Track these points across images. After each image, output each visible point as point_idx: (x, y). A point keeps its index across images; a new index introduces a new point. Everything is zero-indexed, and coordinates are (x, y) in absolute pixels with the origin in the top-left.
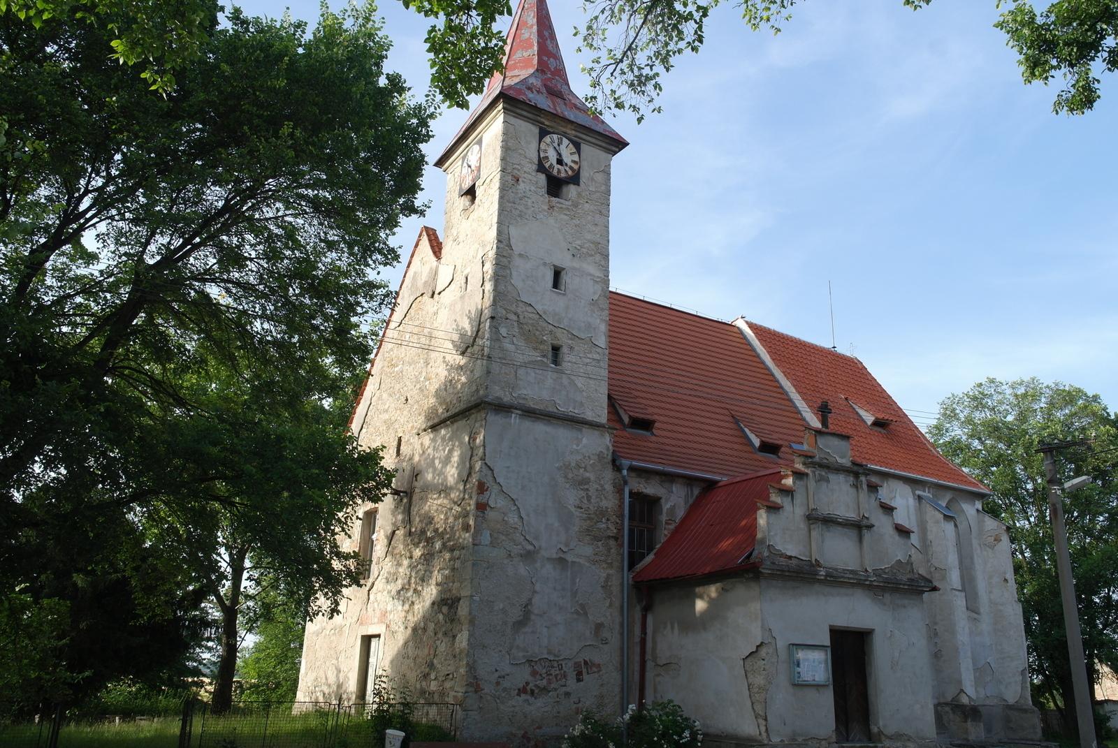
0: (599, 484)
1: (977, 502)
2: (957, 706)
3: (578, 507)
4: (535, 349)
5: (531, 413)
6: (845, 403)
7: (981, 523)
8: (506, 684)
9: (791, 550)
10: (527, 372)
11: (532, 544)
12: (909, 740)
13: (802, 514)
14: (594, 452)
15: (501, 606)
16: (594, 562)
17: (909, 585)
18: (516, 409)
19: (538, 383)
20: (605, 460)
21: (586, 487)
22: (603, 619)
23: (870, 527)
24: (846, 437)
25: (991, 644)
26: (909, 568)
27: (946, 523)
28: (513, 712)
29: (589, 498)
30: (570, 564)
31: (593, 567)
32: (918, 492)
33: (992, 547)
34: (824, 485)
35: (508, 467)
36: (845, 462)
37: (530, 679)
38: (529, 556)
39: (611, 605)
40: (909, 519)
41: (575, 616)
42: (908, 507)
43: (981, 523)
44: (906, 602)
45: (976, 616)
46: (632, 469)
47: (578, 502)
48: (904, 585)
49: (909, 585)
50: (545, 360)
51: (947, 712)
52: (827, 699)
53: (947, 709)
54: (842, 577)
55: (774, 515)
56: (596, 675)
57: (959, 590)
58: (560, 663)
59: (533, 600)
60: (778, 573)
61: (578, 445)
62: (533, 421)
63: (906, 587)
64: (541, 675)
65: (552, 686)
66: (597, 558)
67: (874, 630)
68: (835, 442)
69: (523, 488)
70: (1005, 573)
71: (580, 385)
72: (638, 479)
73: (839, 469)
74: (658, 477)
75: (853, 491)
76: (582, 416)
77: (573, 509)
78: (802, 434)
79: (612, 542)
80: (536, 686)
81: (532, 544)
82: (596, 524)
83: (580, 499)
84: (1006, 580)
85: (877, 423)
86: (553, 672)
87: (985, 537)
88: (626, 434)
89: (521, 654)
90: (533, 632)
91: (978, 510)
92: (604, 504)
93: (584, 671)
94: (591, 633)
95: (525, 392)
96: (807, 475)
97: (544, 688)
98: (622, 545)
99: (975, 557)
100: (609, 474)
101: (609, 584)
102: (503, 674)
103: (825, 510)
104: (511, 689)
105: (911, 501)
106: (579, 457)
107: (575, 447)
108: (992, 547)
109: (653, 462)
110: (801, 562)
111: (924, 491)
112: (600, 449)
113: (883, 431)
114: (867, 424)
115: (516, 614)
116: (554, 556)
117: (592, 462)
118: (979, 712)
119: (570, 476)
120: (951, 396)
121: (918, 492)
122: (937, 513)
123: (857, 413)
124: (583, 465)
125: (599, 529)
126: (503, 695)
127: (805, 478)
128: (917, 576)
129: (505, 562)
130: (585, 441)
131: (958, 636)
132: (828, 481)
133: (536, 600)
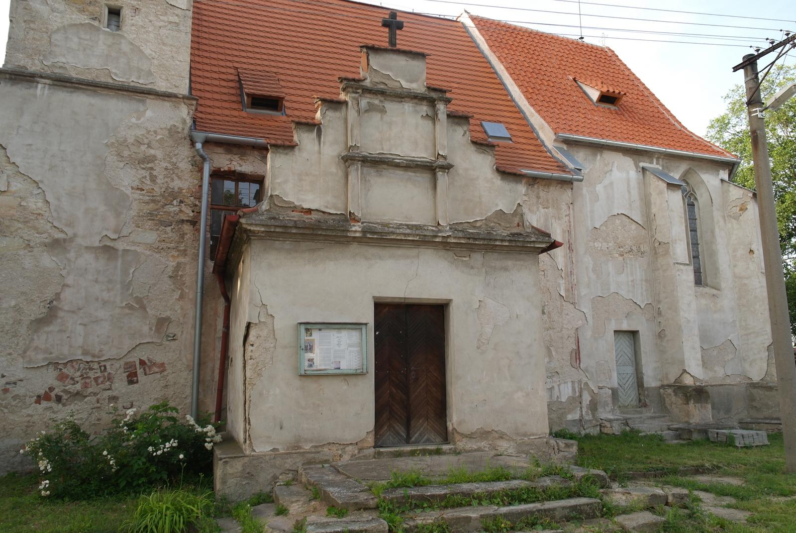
0: (170, 162)
1: (721, 172)
2: (680, 388)
3: (138, 189)
4: (82, 11)
5: (62, 82)
6: (574, 83)
7: (725, 194)
8: (19, 390)
9: (311, 201)
10: (66, 38)
11: (62, 231)
12: (502, 438)
13: (335, 153)
14: (163, 126)
15: (13, 303)
16: (158, 250)
17: (510, 241)
18: (41, 77)
19: (84, 50)
20: (180, 135)
21: (149, 165)
22: (168, 313)
23: (447, 168)
24: (421, 56)
25: (734, 321)
26: (516, 220)
27: (669, 191)
28: (29, 422)
29: (153, 179)
30: (120, 253)
31: (157, 256)
32: (642, 164)
33: (737, 218)
34: (376, 117)
35: (30, 145)
36: (418, 87)
37: (56, 383)
38: (56, 245)
39: (182, 297)
40: (629, 192)
41: (127, 311)
42: (628, 180)
43: (725, 194)
44: (510, 263)
45: (715, 292)
46: (207, 142)
47: (136, 183)
48: (502, 241)
49: (510, 241)
50: (96, 23)
51: (670, 395)
52: (365, 392)
53: (670, 391)
54: (393, 233)
55: (283, 156)
56: (158, 376)
57: (685, 264)
58: (103, 364)
59: (62, 296)
60: (278, 230)
61: (138, 119)
62: (71, 92)
63: (507, 244)
64: (72, 379)
65: (90, 390)
66: (164, 245)
67: (451, 300)
68: (401, 61)
69: (52, 168)
70: (750, 244)
71: (148, 52)
72: (229, 156)
73: (401, 96)
74: (256, 153)
75: (428, 124)
76: (149, 87)
77: (129, 191)
78: (359, 54)
79: (187, 228)
80: (65, 391)
81: (62, 231)
82: (163, 207)
83: (140, 180)
84: (751, 251)
85: (606, 98)
86: (92, 374)
87: (729, 208)
88: (243, 114)
89: (41, 356)
90: (60, 331)
91: (722, 181)
92: (177, 184)
93: (140, 371)
94: (151, 329)
95: (64, 60)
96: (345, 103)
97: (78, 393)
98: (198, 230)
99: (717, 230)
100: (185, 152)
101: (180, 273)
102: (13, 379)
103: (373, 149)
104: (25, 396)
105: (633, 174)
106: (139, 132)
107: (134, 120)
108: (737, 218)
109: (242, 135)
110: (326, 217)
111: (651, 163)
112: (172, 123)
113: (613, 108)
114: (591, 100)
115: (36, 311)
116: (97, 244)
117: (158, 137)
118: (707, 392)
119: (126, 153)
120: (735, 88)
121: (642, 164)
122: (660, 182)
123: (585, 93)
124: (146, 141)
125: (169, 213)
126: (14, 403)
127: (344, 108)
128: (529, 230)
129: (22, 252)
130: (149, 113)
131: (682, 313)
132: (383, 111)
133: (67, 295)
